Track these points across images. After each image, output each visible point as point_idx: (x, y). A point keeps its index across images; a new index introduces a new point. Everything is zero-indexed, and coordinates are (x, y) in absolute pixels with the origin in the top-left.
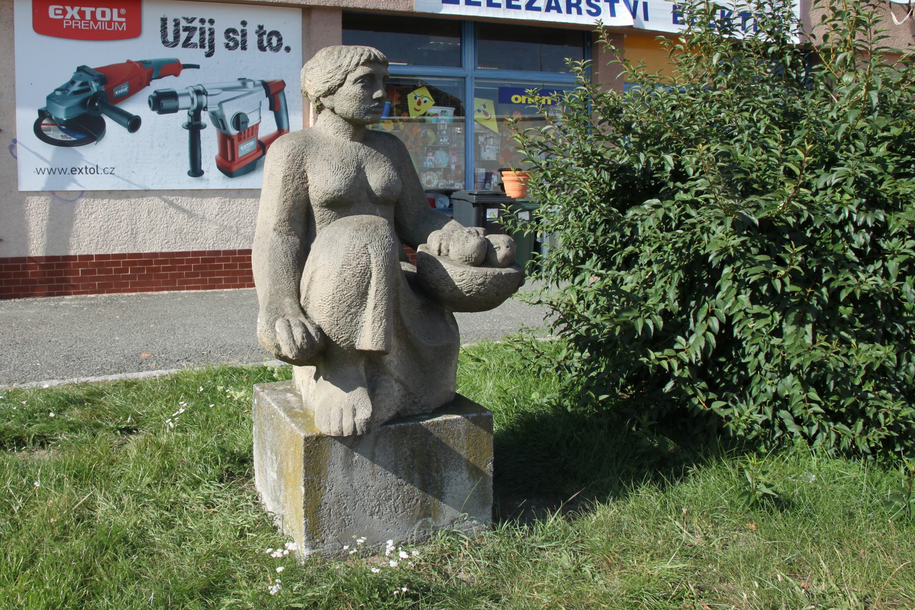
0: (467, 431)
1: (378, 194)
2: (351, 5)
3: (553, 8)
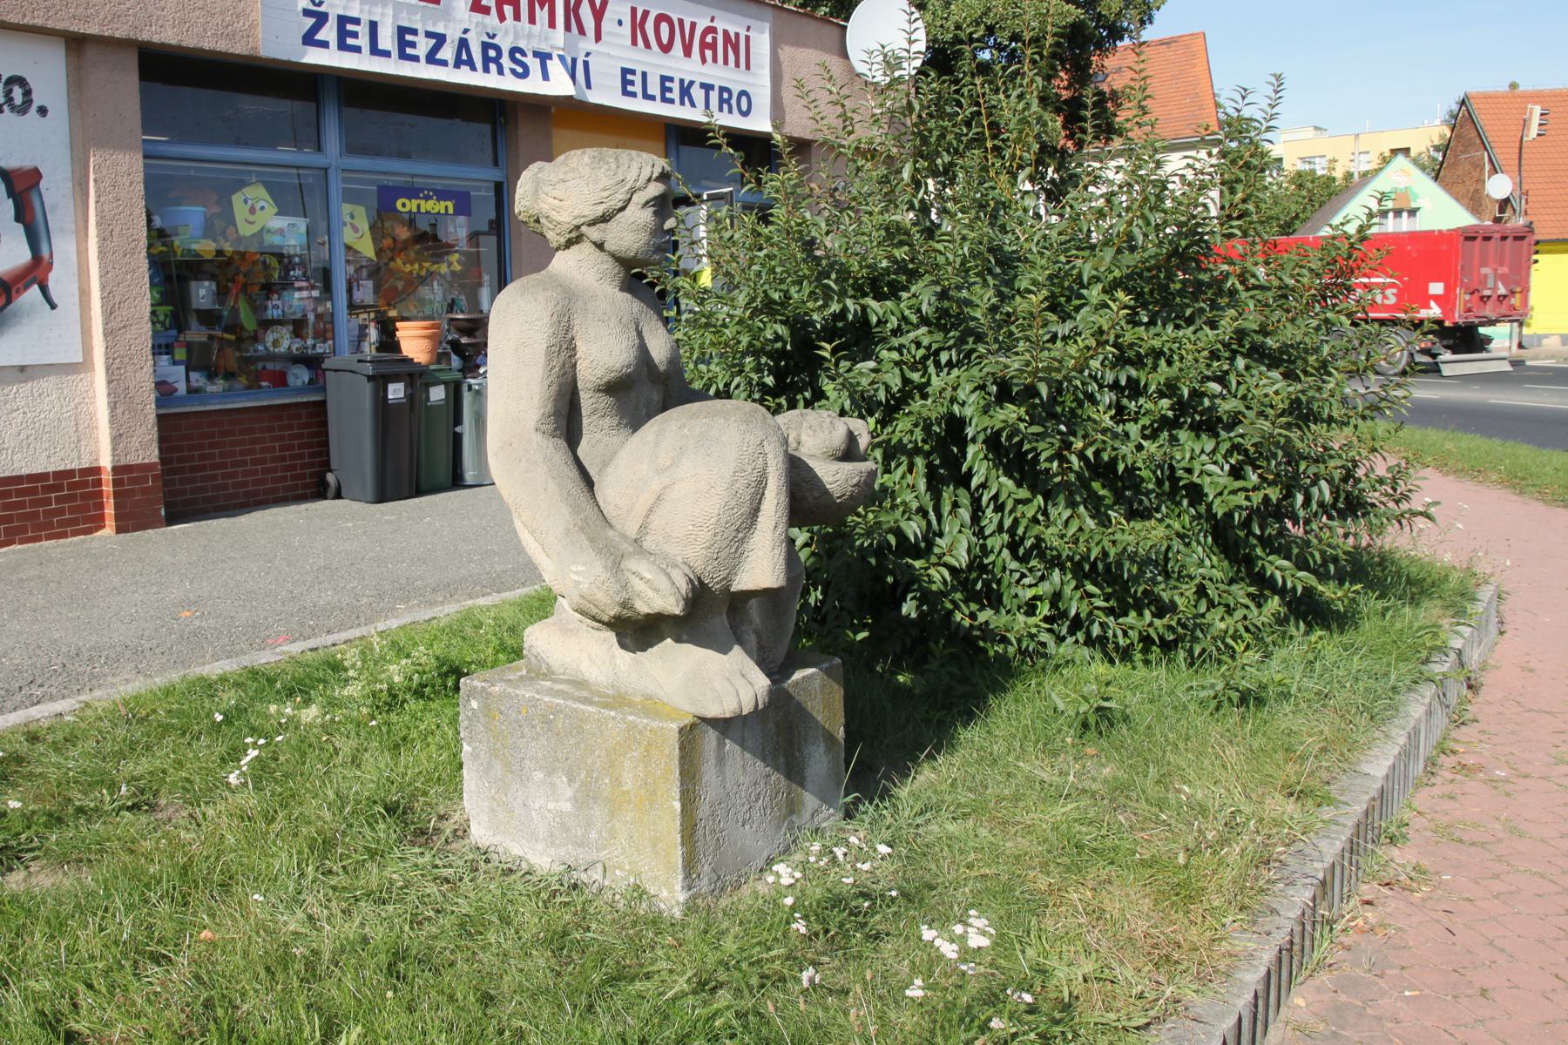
0: (823, 686)
1: (662, 368)
2: (156, 39)
3: (465, 63)
